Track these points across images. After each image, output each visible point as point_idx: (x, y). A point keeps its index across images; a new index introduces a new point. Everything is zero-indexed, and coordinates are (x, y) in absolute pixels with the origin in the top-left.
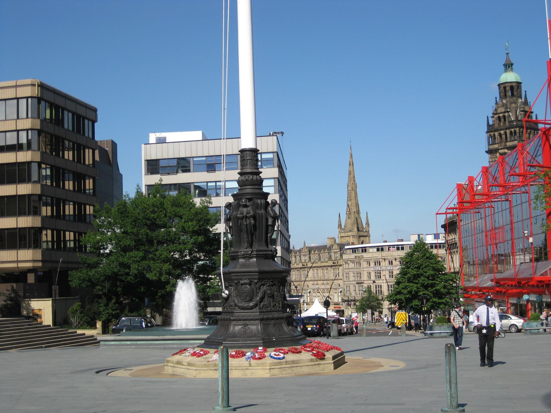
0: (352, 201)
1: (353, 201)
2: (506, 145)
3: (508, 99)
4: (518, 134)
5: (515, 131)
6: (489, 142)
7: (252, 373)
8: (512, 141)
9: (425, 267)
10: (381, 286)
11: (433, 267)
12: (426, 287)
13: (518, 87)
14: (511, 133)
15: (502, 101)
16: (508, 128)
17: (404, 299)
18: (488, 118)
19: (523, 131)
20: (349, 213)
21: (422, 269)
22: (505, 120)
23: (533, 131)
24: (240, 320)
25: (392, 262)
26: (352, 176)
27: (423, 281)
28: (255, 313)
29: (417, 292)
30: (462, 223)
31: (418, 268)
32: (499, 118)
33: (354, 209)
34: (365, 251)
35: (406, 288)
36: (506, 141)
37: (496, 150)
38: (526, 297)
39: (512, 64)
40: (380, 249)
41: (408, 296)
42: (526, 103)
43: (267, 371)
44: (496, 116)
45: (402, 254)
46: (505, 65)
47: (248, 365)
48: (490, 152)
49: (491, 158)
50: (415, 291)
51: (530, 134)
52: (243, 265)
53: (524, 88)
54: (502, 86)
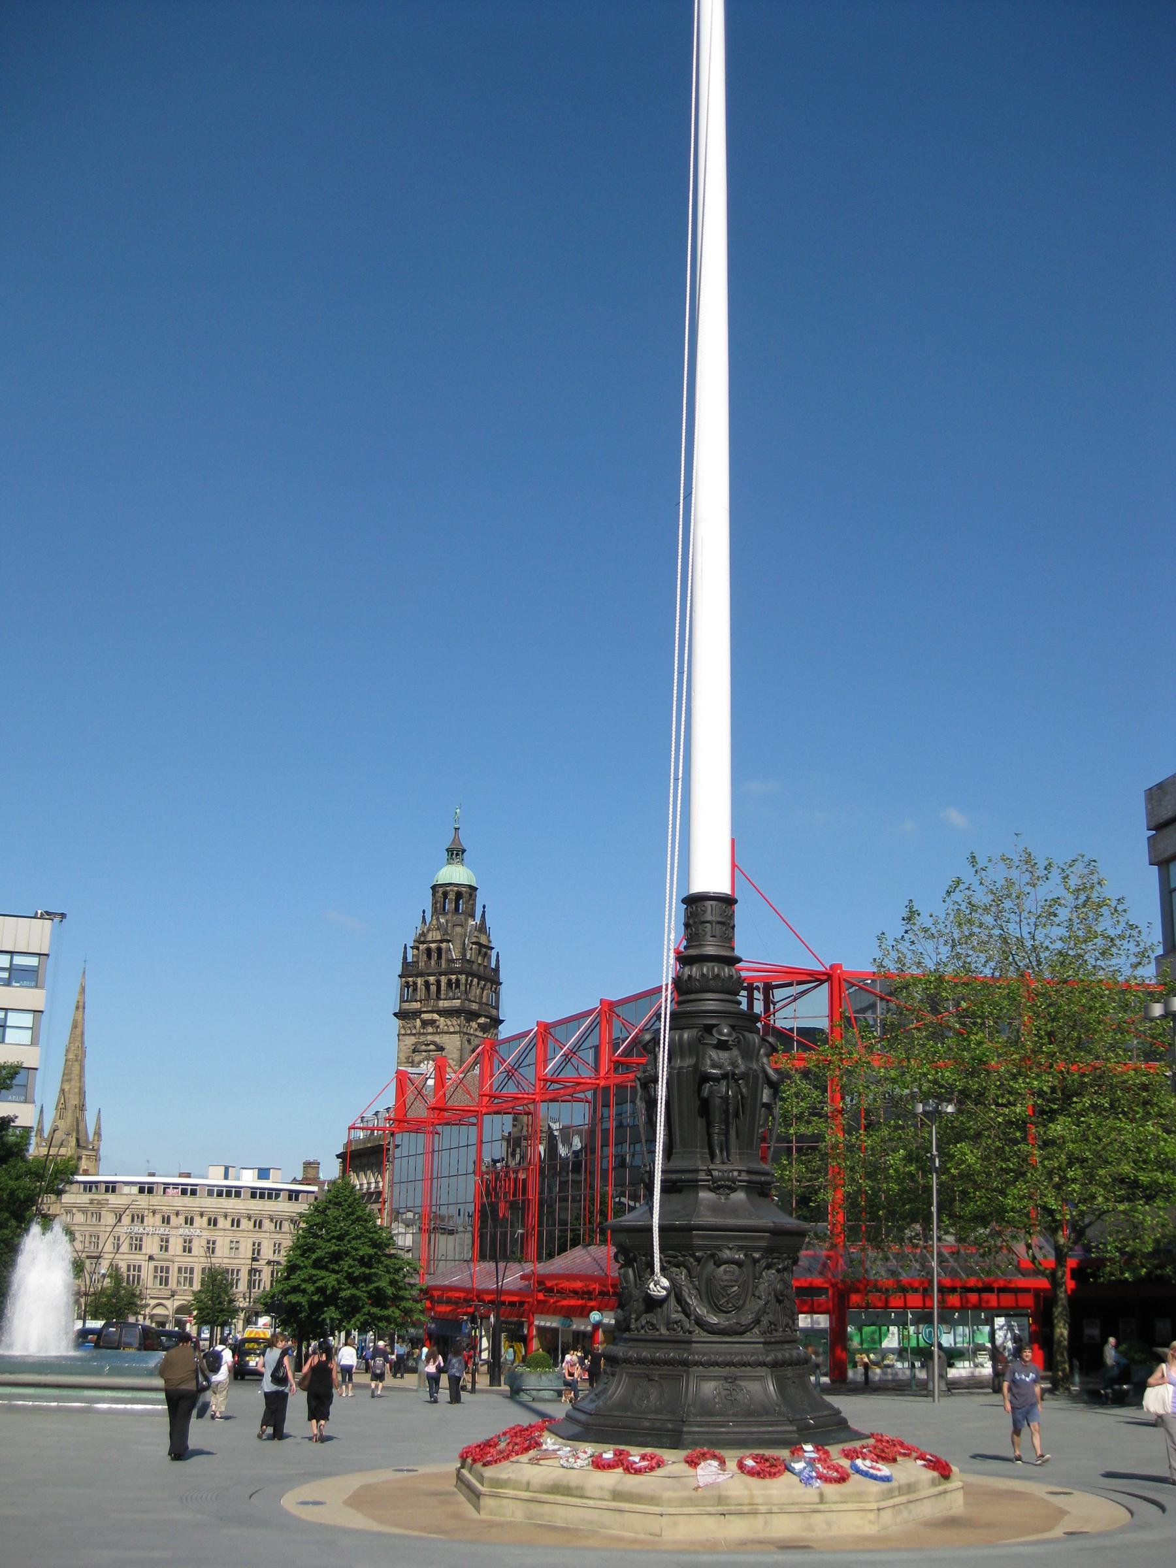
0: (73, 1083)
1: (75, 1083)
3: (449, 917)
4: (462, 988)
5: (458, 980)
6: (402, 996)
7: (829, 1524)
10: (140, 1267)
11: (371, 1239)
12: (353, 1280)
13: (471, 895)
15: (438, 919)
17: (305, 1304)
18: (405, 948)
20: (62, 1108)
21: (349, 1242)
22: (439, 957)
23: (489, 985)
24: (717, 1364)
25: (169, 1218)
26: (78, 1030)
27: (350, 1267)
28: (751, 1346)
29: (336, 1291)
30: (398, 1152)
31: (340, 1238)
32: (429, 950)
33: (74, 1101)
34: (114, 1190)
35: (311, 1279)
36: (438, 998)
37: (416, 1014)
38: (595, 1316)
39: (464, 851)
40: (146, 1189)
41: (315, 1298)
42: (482, 928)
43: (872, 1516)
44: (422, 947)
45: (302, 1207)
46: (450, 851)
47: (817, 1499)
48: (401, 1015)
50: (333, 1287)
51: (483, 989)
52: (715, 1209)
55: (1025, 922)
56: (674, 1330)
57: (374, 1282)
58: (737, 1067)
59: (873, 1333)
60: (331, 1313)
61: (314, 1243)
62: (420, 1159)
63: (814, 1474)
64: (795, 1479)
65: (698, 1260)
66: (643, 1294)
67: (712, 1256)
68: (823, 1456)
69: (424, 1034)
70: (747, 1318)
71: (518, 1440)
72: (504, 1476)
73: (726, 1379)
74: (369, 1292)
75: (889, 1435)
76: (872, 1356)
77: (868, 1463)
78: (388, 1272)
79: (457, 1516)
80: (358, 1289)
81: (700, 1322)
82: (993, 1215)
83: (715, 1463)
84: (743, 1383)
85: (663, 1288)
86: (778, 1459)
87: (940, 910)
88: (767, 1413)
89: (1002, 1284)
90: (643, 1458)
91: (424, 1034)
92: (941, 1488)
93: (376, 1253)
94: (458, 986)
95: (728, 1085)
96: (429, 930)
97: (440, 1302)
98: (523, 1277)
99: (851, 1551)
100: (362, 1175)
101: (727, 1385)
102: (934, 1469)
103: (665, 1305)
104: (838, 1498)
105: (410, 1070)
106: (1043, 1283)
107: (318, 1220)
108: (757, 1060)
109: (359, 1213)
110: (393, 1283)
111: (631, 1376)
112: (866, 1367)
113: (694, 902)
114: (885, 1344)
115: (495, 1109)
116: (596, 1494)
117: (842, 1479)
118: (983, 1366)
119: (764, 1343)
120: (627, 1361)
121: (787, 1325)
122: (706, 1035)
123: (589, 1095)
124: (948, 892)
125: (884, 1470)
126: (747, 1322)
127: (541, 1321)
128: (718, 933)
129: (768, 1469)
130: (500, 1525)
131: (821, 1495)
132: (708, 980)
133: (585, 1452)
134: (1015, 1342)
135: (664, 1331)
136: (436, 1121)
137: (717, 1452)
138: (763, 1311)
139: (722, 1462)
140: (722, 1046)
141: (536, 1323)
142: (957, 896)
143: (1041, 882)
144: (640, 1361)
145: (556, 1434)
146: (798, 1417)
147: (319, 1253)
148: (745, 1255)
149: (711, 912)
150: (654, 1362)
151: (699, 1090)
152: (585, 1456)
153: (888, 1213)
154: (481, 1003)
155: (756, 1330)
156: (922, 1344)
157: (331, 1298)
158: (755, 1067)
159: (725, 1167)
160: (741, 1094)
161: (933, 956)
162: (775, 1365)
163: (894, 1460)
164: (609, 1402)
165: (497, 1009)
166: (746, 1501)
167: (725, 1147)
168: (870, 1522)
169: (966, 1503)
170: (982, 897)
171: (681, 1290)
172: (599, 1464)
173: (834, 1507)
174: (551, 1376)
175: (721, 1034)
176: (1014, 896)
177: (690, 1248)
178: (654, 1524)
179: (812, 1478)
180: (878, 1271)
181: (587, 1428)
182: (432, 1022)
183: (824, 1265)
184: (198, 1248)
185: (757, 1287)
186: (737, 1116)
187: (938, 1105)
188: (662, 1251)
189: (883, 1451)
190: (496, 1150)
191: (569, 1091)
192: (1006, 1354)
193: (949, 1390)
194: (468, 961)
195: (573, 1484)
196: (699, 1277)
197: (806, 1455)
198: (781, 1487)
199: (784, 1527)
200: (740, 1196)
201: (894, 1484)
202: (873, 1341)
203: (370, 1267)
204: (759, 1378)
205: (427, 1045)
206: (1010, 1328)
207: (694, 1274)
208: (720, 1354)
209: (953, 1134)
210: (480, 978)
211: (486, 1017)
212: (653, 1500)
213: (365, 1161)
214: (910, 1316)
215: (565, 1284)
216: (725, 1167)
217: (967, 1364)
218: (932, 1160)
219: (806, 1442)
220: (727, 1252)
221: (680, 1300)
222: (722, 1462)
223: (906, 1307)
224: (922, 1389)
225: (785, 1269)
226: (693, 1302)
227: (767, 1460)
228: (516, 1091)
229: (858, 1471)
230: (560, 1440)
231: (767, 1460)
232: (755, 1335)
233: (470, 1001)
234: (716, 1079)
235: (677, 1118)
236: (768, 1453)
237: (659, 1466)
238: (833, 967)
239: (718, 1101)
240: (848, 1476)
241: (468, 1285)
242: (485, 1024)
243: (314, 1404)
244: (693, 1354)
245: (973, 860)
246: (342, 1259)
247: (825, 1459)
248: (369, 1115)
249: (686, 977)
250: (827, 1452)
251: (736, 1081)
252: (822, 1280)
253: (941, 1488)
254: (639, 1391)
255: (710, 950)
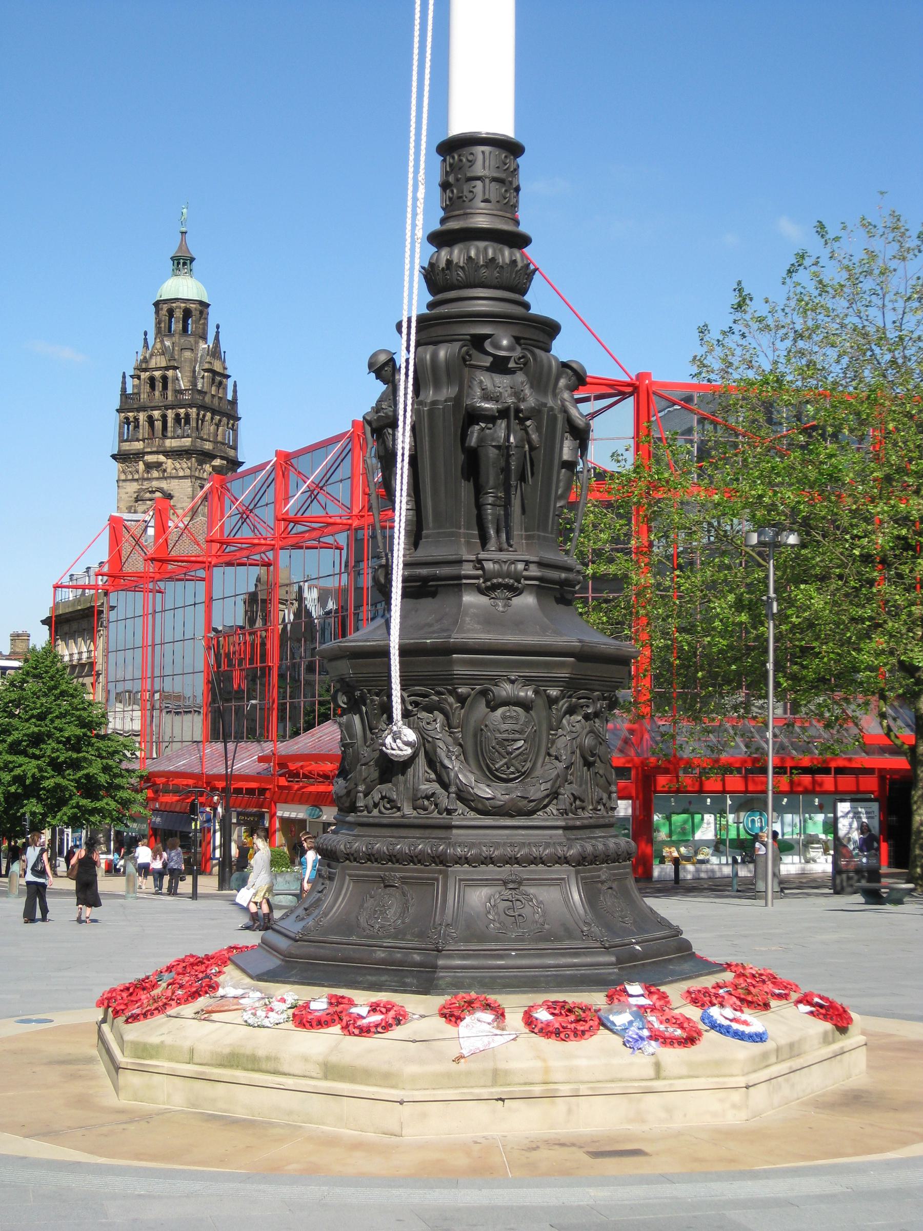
2: (163, 445)
3: (176, 339)
4: (193, 424)
5: (187, 415)
6: (121, 434)
7: (669, 1110)
8: (178, 437)
9: (57, 717)
11: (79, 718)
12: (57, 767)
13: (201, 312)
14: (177, 418)
15: (162, 342)
16: (172, 407)
18: (124, 377)
19: (204, 416)
21: (52, 721)
22: (165, 387)
23: (225, 420)
24: (489, 860)
27: (54, 750)
28: (544, 833)
29: (37, 781)
30: (113, 615)
31: (41, 717)
32: (152, 380)
36: (164, 436)
37: (138, 456)
39: (192, 260)
41: (12, 789)
42: (216, 352)
43: (736, 1097)
44: (144, 375)
47: (651, 1073)
48: (121, 457)
49: (124, 472)
50: (33, 776)
51: (218, 425)
52: (489, 620)
53: (214, 317)
54: (165, 307)
55: (889, 306)
56: (425, 809)
57: (84, 768)
58: (524, 400)
59: (685, 822)
60: (32, 807)
61: (9, 724)
63: (646, 1033)
64: (617, 1040)
65: (462, 699)
66: (376, 755)
67: (484, 693)
68: (659, 1004)
69: (148, 479)
70: (538, 790)
71: (185, 980)
72: (154, 1040)
73: (505, 883)
74: (77, 781)
75: (754, 965)
76: (683, 850)
77: (729, 1012)
78: (100, 756)
79: (83, 1102)
80: (64, 778)
81: (464, 797)
82: (843, 678)
83: (488, 1017)
84: (532, 890)
85: (407, 744)
86: (586, 1009)
87: (779, 295)
88: (570, 935)
89: (841, 763)
90: (374, 1008)
91: (148, 479)
92: (836, 1047)
93: (85, 735)
94: (187, 421)
95: (508, 427)
96: (152, 355)
97: (167, 792)
98: (261, 759)
99: (719, 1177)
100: (71, 642)
101: (507, 894)
102: (826, 1017)
103: (410, 771)
104: (684, 1071)
105: (126, 516)
106: (901, 762)
107: (14, 696)
108: (555, 395)
109: (64, 687)
110: (106, 769)
111: (357, 880)
112: (676, 862)
113: (454, 149)
114: (699, 835)
115: (227, 559)
116: (297, 1068)
117: (690, 1040)
118: (815, 861)
119: (565, 828)
120: (351, 857)
121: (600, 801)
122: (473, 352)
123: (342, 539)
124: (789, 272)
125: (754, 1022)
126: (540, 795)
127: (286, 812)
128: (493, 197)
129: (573, 1025)
130: (147, 1117)
131: (658, 1066)
132: (478, 268)
133: (283, 1000)
134: (862, 833)
135: (408, 810)
136: (158, 576)
137: (492, 998)
138: (565, 779)
139: (500, 1014)
140: (500, 366)
141: (279, 814)
142: (802, 276)
143: (910, 256)
144: (372, 857)
145: (244, 971)
146: (618, 941)
147: (16, 735)
148: (536, 692)
149: (483, 162)
150: (393, 858)
151: (464, 436)
152: (283, 1006)
153: (706, 676)
154: (215, 442)
155: (552, 809)
156: (743, 835)
157: (32, 789)
158: (550, 403)
159: (503, 556)
160: (530, 442)
161: (768, 354)
162: (582, 861)
163: (766, 1006)
164: (325, 921)
165: (235, 448)
166: (539, 1078)
167: (504, 525)
168: (734, 1106)
169: (870, 1067)
170: (833, 274)
171: (435, 747)
172: (304, 1019)
173: (679, 1084)
174: (288, 877)
175: (498, 347)
176: (876, 272)
177: (449, 681)
178: (390, 1117)
179: (642, 1038)
180: (692, 746)
181: (304, 956)
182: (158, 465)
183: (626, 741)
185: (553, 742)
186: (522, 478)
187: (777, 534)
188: (404, 687)
189: (749, 993)
190: (231, 614)
191: (315, 534)
192: (851, 847)
193: (782, 890)
194: (200, 392)
195: (261, 1053)
196: (463, 725)
197: (633, 1001)
198: (595, 1053)
199: (599, 1118)
200: (528, 600)
201: (769, 1045)
202: (683, 831)
203: (79, 751)
204: (558, 882)
205: (152, 492)
206: (857, 816)
207: (455, 721)
208: (497, 845)
209: (797, 573)
210: (214, 412)
211: (222, 458)
212: (387, 1078)
213: (75, 626)
214: (729, 802)
215: (313, 766)
216: (503, 556)
217: (796, 859)
218: (769, 604)
219: (631, 981)
220: (508, 687)
221: (433, 762)
222: (500, 1014)
223: (724, 792)
224: (747, 890)
225: (596, 715)
226: (453, 765)
227: (570, 1011)
228: (251, 535)
229: (714, 1026)
230: (248, 980)
231: (570, 1011)
232: (550, 815)
233: (202, 439)
234: (491, 419)
235: (428, 480)
236: (572, 998)
237: (399, 1022)
238: (641, 376)
239: (492, 453)
240: (699, 1033)
241: (197, 770)
242: (221, 467)
244: (454, 845)
245: (821, 229)
246: (44, 742)
247: (662, 1005)
248: (79, 570)
249: (442, 264)
250: (663, 996)
251: (522, 421)
252: (623, 760)
253: (836, 1047)
254: (370, 903)
255: (482, 222)
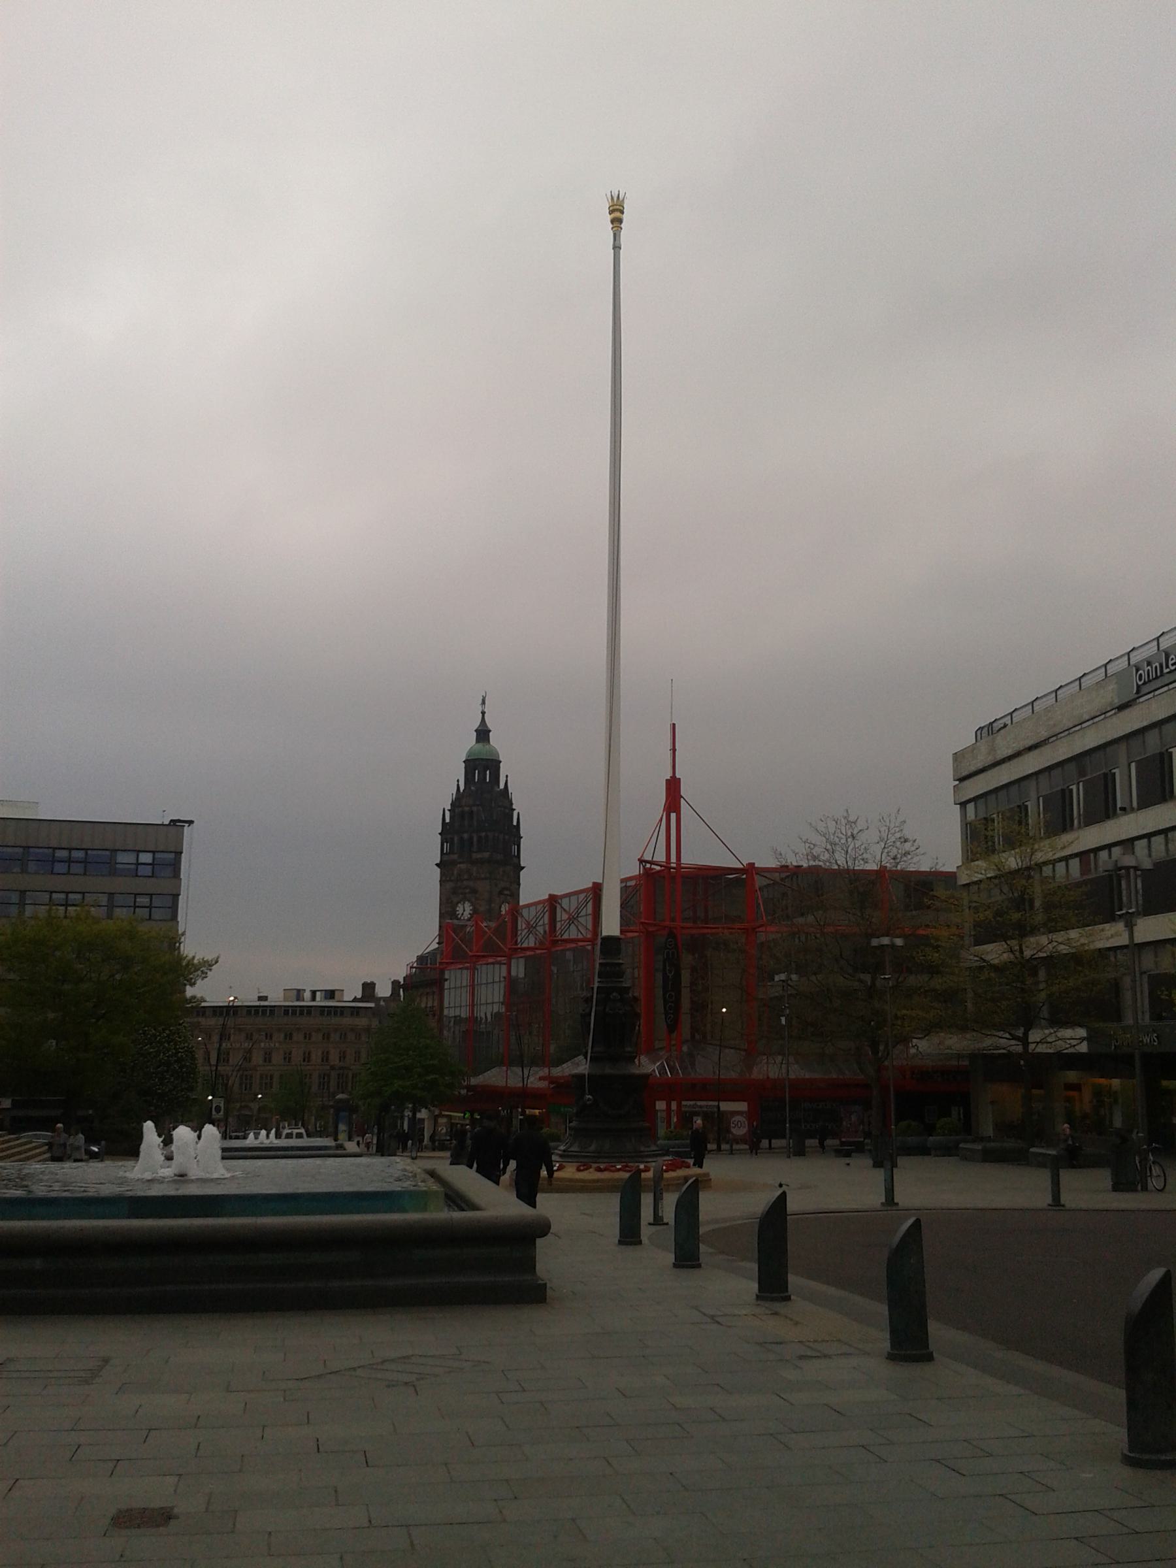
62: (464, 990)
184: (277, 1058)
243: (449, 885)
